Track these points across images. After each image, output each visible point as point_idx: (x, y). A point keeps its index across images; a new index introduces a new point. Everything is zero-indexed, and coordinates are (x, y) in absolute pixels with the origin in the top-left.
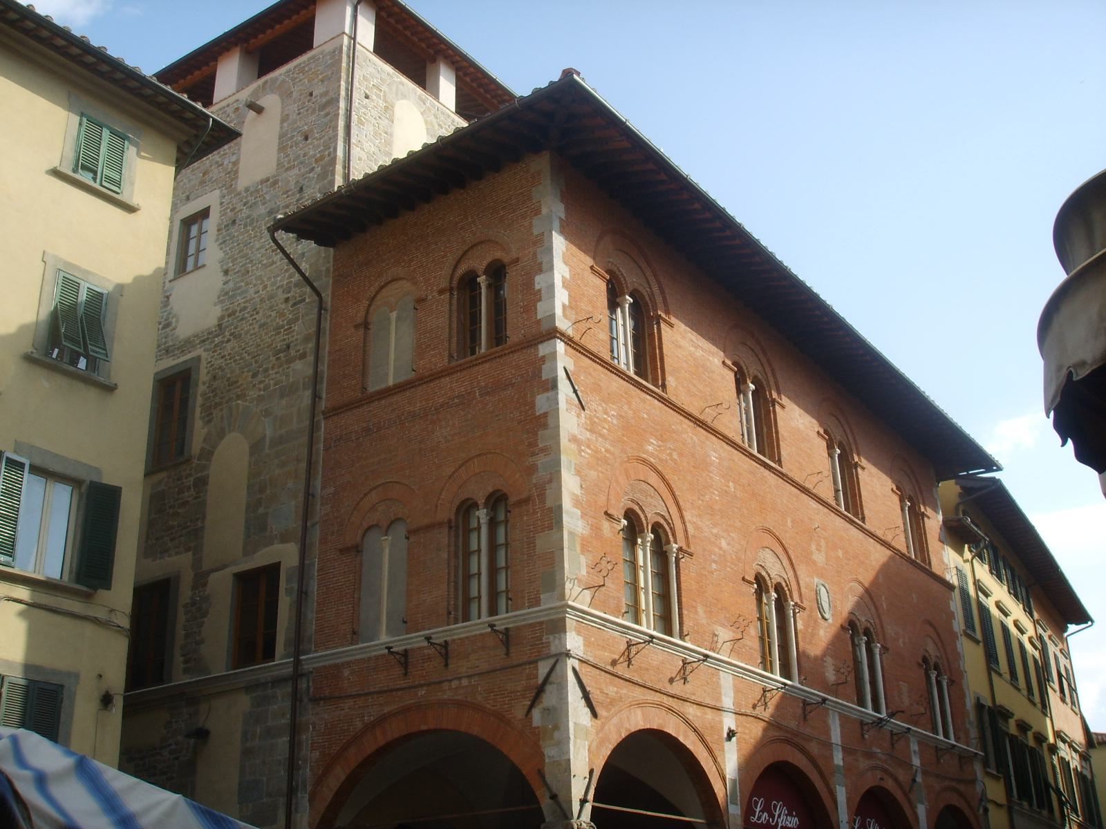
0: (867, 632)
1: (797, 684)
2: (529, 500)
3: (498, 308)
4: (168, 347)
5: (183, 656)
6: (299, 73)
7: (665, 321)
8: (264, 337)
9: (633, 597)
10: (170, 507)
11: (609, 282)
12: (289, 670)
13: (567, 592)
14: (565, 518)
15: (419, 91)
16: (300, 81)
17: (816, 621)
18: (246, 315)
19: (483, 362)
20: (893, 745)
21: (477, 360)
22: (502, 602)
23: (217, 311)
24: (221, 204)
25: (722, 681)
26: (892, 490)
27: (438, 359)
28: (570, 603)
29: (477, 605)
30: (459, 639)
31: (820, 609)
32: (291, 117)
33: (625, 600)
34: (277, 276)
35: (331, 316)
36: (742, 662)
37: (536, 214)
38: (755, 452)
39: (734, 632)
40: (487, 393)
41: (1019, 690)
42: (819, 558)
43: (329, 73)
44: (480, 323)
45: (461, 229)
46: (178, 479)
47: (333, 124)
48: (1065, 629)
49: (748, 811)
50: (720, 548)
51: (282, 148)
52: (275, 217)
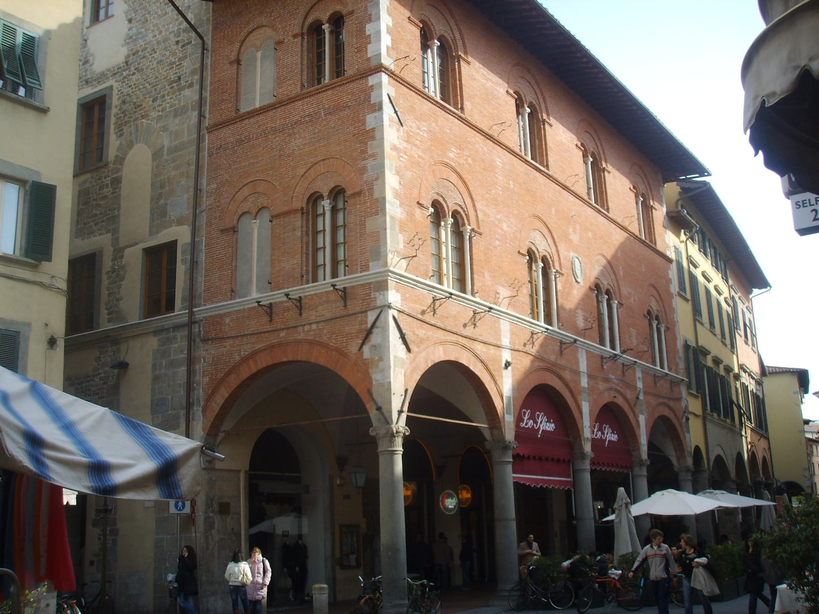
3: (338, 49)
7: (464, 60)
8: (161, 71)
9: (438, 265)
10: (94, 200)
11: (422, 29)
12: (185, 319)
13: (389, 261)
14: (388, 206)
17: (571, 284)
18: (147, 54)
23: (124, 51)
25: (502, 327)
26: (630, 189)
28: (391, 269)
30: (309, 296)
33: (432, 266)
34: (170, 23)
38: (529, 158)
39: (511, 291)
40: (330, 113)
41: (715, 335)
42: (575, 238)
44: (325, 60)
46: (99, 179)
48: (751, 292)
49: (519, 419)
50: (502, 230)
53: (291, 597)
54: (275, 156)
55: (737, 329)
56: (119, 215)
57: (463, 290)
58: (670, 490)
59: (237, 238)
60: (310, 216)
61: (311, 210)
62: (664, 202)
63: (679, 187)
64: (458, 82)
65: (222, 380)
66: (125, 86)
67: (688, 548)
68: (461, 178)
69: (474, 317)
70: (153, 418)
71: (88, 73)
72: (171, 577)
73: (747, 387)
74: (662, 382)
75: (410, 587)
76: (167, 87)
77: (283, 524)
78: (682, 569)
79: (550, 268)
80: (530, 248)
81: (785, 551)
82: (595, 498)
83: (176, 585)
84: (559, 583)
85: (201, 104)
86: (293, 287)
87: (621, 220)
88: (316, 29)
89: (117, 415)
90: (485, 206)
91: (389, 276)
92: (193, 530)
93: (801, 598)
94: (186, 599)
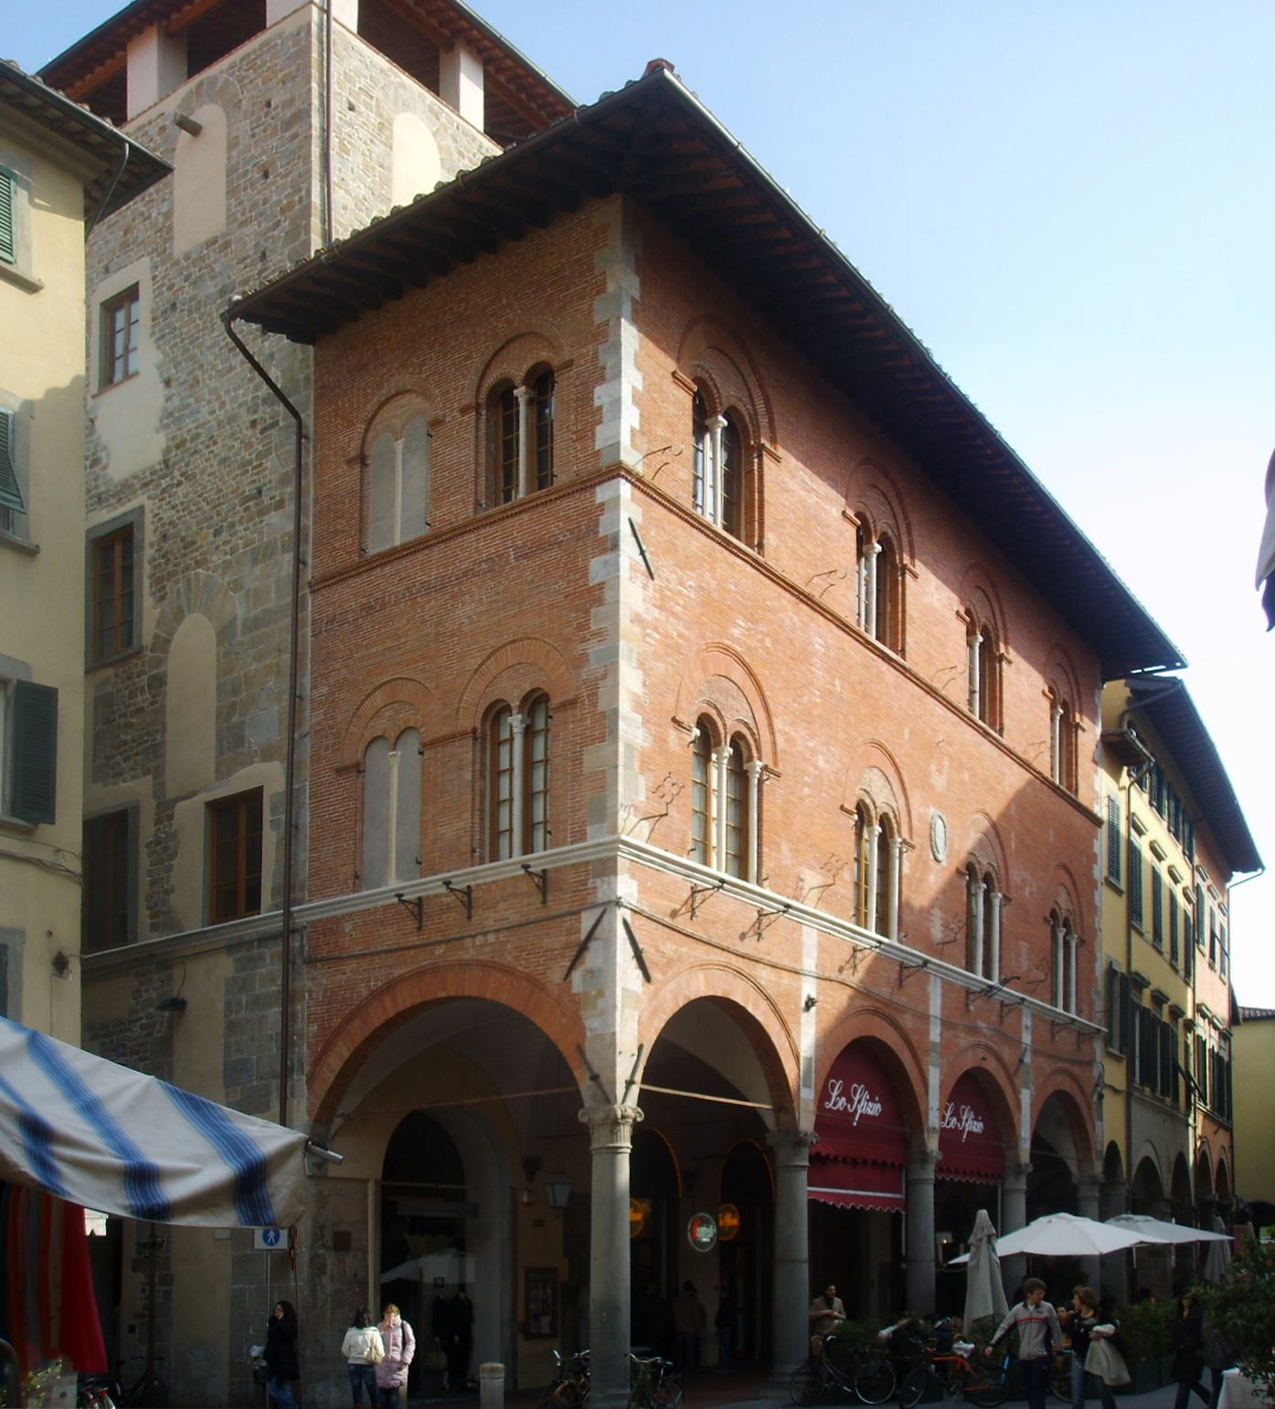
0: (987, 878)
1: (895, 942)
2: (576, 703)
3: (542, 434)
4: (102, 493)
5: (148, 908)
6: (248, 69)
7: (770, 453)
8: (226, 479)
9: (702, 831)
10: (121, 716)
11: (696, 396)
12: (278, 925)
13: (620, 823)
14: (622, 726)
15: (429, 97)
16: (251, 82)
17: (926, 863)
18: (200, 446)
19: (520, 512)
20: (1001, 1017)
21: (512, 508)
22: (539, 836)
23: (161, 441)
24: (154, 278)
25: (805, 938)
26: (1043, 692)
27: (460, 509)
28: (624, 837)
29: (507, 839)
30: (485, 884)
31: (933, 847)
32: (241, 141)
33: (692, 832)
34: (239, 387)
35: (315, 447)
36: (830, 914)
37: (598, 293)
38: (872, 638)
39: (824, 876)
40: (526, 556)
41: (1160, 953)
42: (939, 782)
43: (293, 68)
44: (518, 455)
45: (493, 314)
46: (129, 679)
47: (303, 151)
48: (1227, 878)
49: (823, 1096)
50: (816, 767)
51: (232, 192)
52: (230, 299)
53: (446, 1382)
54: (428, 635)
55: (1198, 942)
56: (164, 741)
57: (743, 874)
58: (1062, 1214)
59: (363, 784)
60: (488, 745)
61: (489, 733)
62: (1100, 716)
63: (1128, 689)
64: (756, 495)
65: (339, 1030)
66: (165, 507)
67: (1084, 1308)
68: (751, 674)
69: (759, 921)
70: (227, 1093)
71: (100, 482)
72: (256, 1350)
73: (1205, 1042)
74: (1064, 1034)
75: (633, 1364)
76: (238, 508)
77: (436, 1267)
78: (1073, 1342)
79: (892, 836)
80: (862, 800)
81: (1241, 1315)
82: (940, 1227)
83: (264, 1363)
84: (872, 1364)
85: (299, 540)
86: (456, 869)
87: (1022, 749)
88: (501, 397)
89: (169, 1089)
90: (790, 725)
91: (619, 849)
92: (292, 1275)
93: (1262, 1391)
94: (280, 1385)
